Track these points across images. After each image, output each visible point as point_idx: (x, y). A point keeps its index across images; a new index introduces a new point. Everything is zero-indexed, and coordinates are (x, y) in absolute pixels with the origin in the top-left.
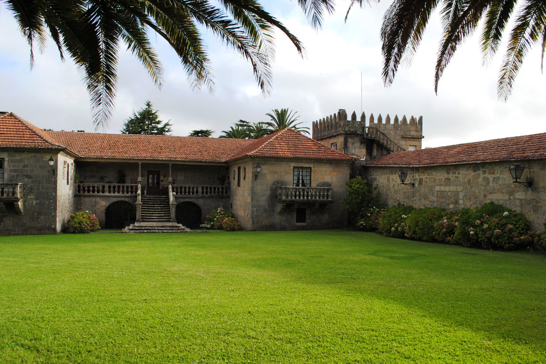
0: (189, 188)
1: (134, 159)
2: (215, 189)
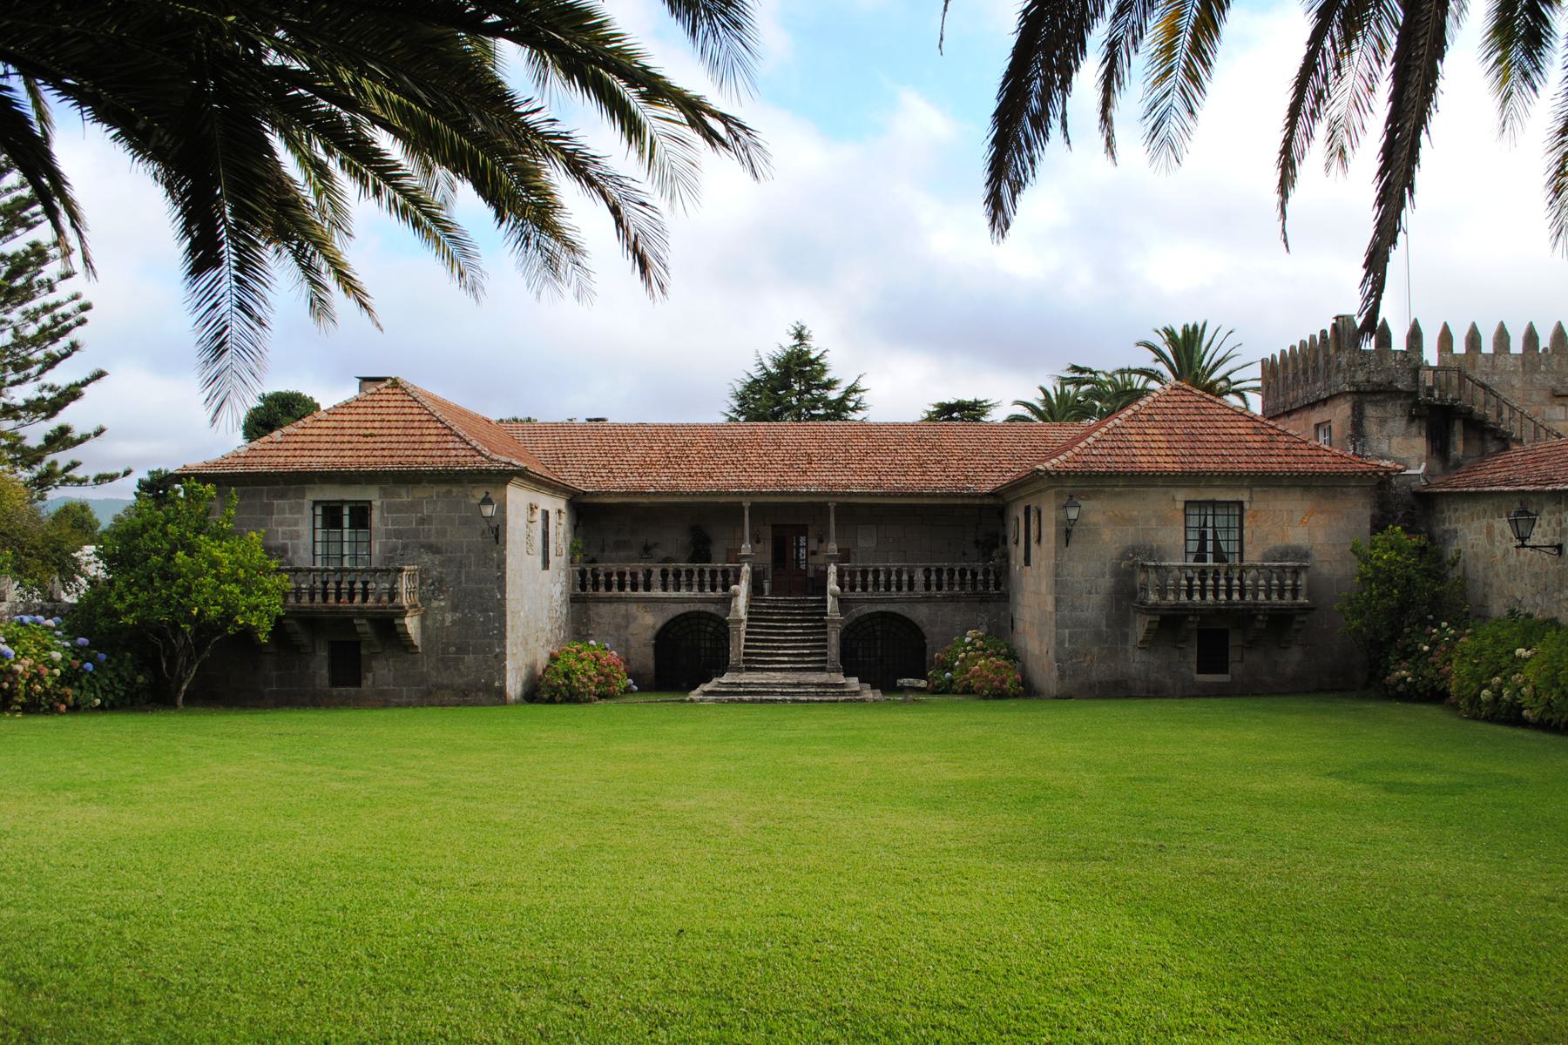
0: (888, 573)
1: (728, 494)
2: (963, 573)
